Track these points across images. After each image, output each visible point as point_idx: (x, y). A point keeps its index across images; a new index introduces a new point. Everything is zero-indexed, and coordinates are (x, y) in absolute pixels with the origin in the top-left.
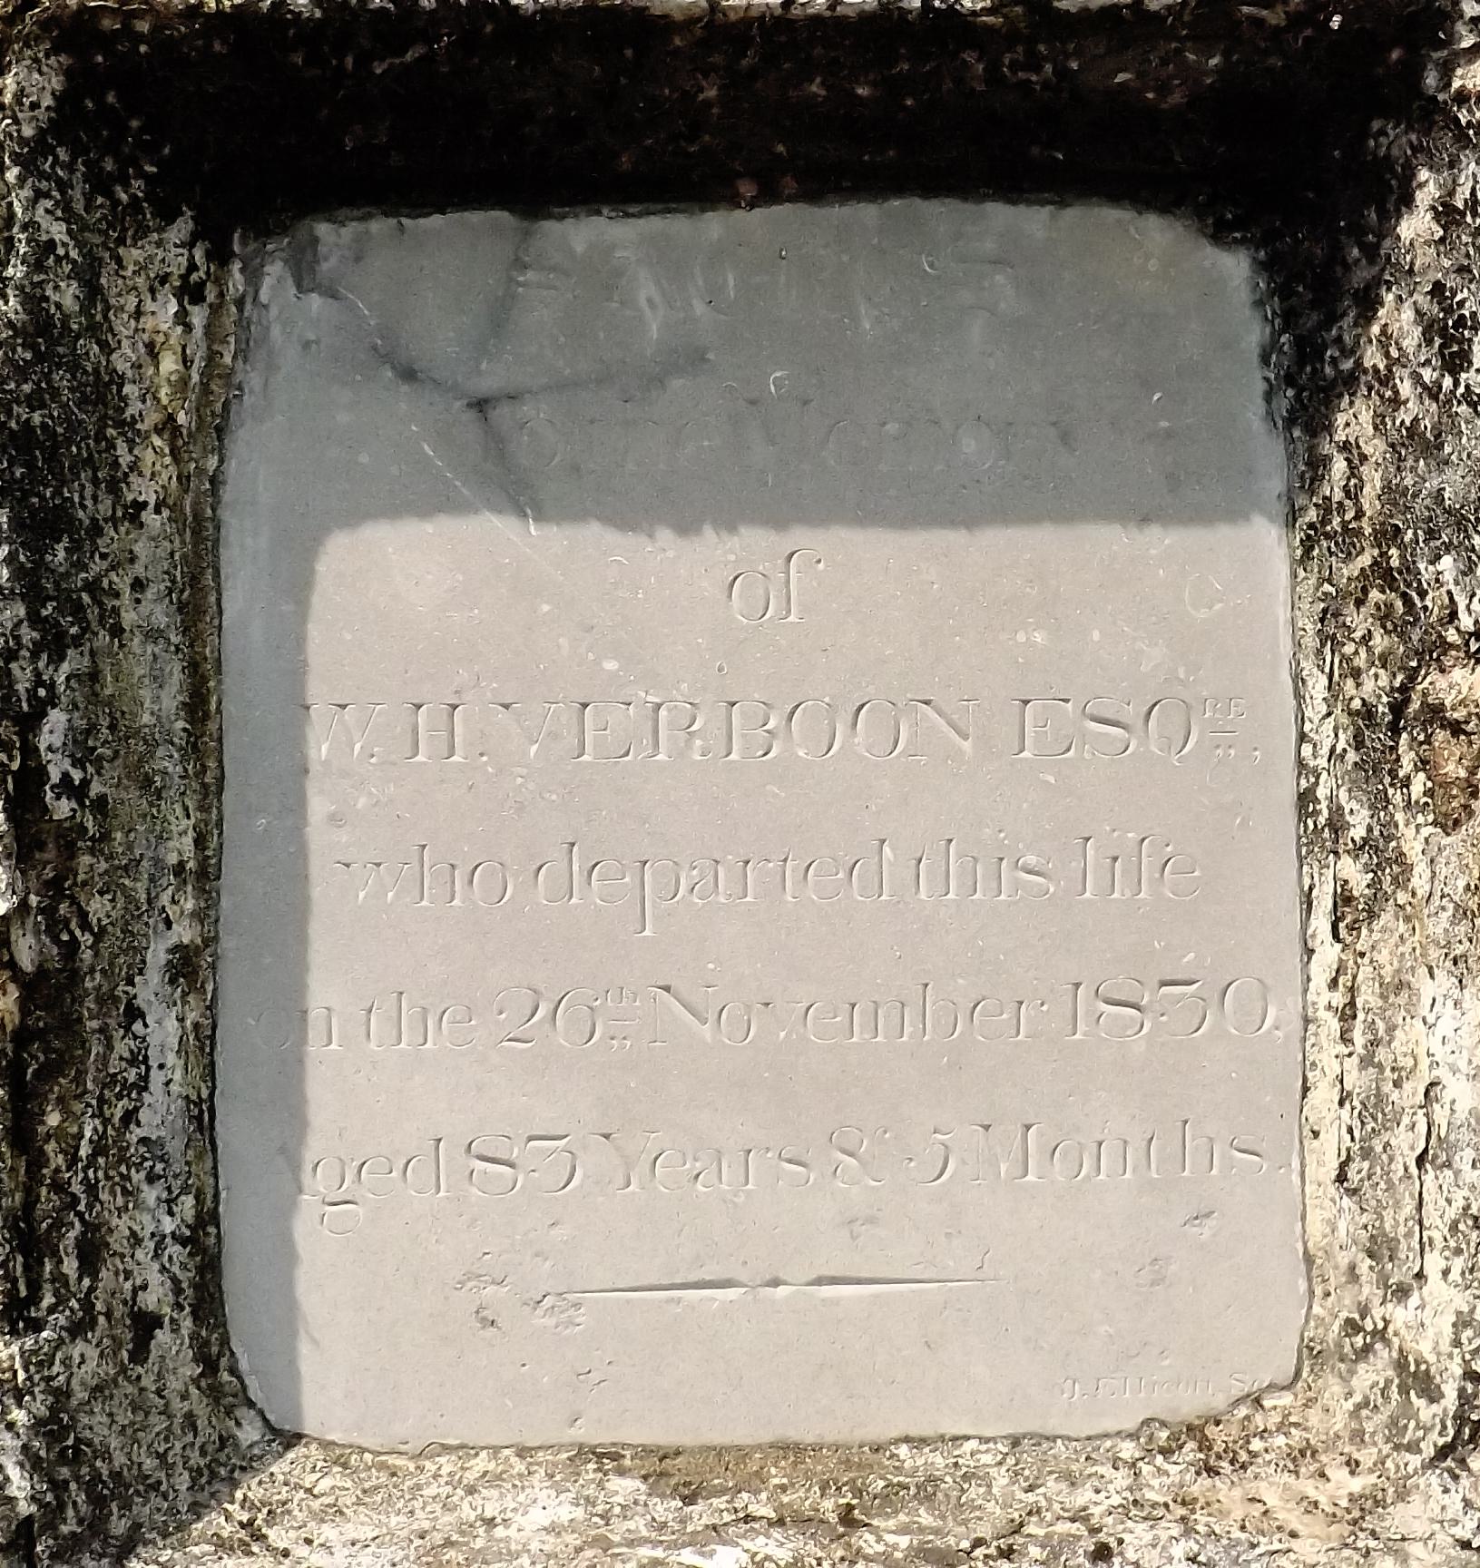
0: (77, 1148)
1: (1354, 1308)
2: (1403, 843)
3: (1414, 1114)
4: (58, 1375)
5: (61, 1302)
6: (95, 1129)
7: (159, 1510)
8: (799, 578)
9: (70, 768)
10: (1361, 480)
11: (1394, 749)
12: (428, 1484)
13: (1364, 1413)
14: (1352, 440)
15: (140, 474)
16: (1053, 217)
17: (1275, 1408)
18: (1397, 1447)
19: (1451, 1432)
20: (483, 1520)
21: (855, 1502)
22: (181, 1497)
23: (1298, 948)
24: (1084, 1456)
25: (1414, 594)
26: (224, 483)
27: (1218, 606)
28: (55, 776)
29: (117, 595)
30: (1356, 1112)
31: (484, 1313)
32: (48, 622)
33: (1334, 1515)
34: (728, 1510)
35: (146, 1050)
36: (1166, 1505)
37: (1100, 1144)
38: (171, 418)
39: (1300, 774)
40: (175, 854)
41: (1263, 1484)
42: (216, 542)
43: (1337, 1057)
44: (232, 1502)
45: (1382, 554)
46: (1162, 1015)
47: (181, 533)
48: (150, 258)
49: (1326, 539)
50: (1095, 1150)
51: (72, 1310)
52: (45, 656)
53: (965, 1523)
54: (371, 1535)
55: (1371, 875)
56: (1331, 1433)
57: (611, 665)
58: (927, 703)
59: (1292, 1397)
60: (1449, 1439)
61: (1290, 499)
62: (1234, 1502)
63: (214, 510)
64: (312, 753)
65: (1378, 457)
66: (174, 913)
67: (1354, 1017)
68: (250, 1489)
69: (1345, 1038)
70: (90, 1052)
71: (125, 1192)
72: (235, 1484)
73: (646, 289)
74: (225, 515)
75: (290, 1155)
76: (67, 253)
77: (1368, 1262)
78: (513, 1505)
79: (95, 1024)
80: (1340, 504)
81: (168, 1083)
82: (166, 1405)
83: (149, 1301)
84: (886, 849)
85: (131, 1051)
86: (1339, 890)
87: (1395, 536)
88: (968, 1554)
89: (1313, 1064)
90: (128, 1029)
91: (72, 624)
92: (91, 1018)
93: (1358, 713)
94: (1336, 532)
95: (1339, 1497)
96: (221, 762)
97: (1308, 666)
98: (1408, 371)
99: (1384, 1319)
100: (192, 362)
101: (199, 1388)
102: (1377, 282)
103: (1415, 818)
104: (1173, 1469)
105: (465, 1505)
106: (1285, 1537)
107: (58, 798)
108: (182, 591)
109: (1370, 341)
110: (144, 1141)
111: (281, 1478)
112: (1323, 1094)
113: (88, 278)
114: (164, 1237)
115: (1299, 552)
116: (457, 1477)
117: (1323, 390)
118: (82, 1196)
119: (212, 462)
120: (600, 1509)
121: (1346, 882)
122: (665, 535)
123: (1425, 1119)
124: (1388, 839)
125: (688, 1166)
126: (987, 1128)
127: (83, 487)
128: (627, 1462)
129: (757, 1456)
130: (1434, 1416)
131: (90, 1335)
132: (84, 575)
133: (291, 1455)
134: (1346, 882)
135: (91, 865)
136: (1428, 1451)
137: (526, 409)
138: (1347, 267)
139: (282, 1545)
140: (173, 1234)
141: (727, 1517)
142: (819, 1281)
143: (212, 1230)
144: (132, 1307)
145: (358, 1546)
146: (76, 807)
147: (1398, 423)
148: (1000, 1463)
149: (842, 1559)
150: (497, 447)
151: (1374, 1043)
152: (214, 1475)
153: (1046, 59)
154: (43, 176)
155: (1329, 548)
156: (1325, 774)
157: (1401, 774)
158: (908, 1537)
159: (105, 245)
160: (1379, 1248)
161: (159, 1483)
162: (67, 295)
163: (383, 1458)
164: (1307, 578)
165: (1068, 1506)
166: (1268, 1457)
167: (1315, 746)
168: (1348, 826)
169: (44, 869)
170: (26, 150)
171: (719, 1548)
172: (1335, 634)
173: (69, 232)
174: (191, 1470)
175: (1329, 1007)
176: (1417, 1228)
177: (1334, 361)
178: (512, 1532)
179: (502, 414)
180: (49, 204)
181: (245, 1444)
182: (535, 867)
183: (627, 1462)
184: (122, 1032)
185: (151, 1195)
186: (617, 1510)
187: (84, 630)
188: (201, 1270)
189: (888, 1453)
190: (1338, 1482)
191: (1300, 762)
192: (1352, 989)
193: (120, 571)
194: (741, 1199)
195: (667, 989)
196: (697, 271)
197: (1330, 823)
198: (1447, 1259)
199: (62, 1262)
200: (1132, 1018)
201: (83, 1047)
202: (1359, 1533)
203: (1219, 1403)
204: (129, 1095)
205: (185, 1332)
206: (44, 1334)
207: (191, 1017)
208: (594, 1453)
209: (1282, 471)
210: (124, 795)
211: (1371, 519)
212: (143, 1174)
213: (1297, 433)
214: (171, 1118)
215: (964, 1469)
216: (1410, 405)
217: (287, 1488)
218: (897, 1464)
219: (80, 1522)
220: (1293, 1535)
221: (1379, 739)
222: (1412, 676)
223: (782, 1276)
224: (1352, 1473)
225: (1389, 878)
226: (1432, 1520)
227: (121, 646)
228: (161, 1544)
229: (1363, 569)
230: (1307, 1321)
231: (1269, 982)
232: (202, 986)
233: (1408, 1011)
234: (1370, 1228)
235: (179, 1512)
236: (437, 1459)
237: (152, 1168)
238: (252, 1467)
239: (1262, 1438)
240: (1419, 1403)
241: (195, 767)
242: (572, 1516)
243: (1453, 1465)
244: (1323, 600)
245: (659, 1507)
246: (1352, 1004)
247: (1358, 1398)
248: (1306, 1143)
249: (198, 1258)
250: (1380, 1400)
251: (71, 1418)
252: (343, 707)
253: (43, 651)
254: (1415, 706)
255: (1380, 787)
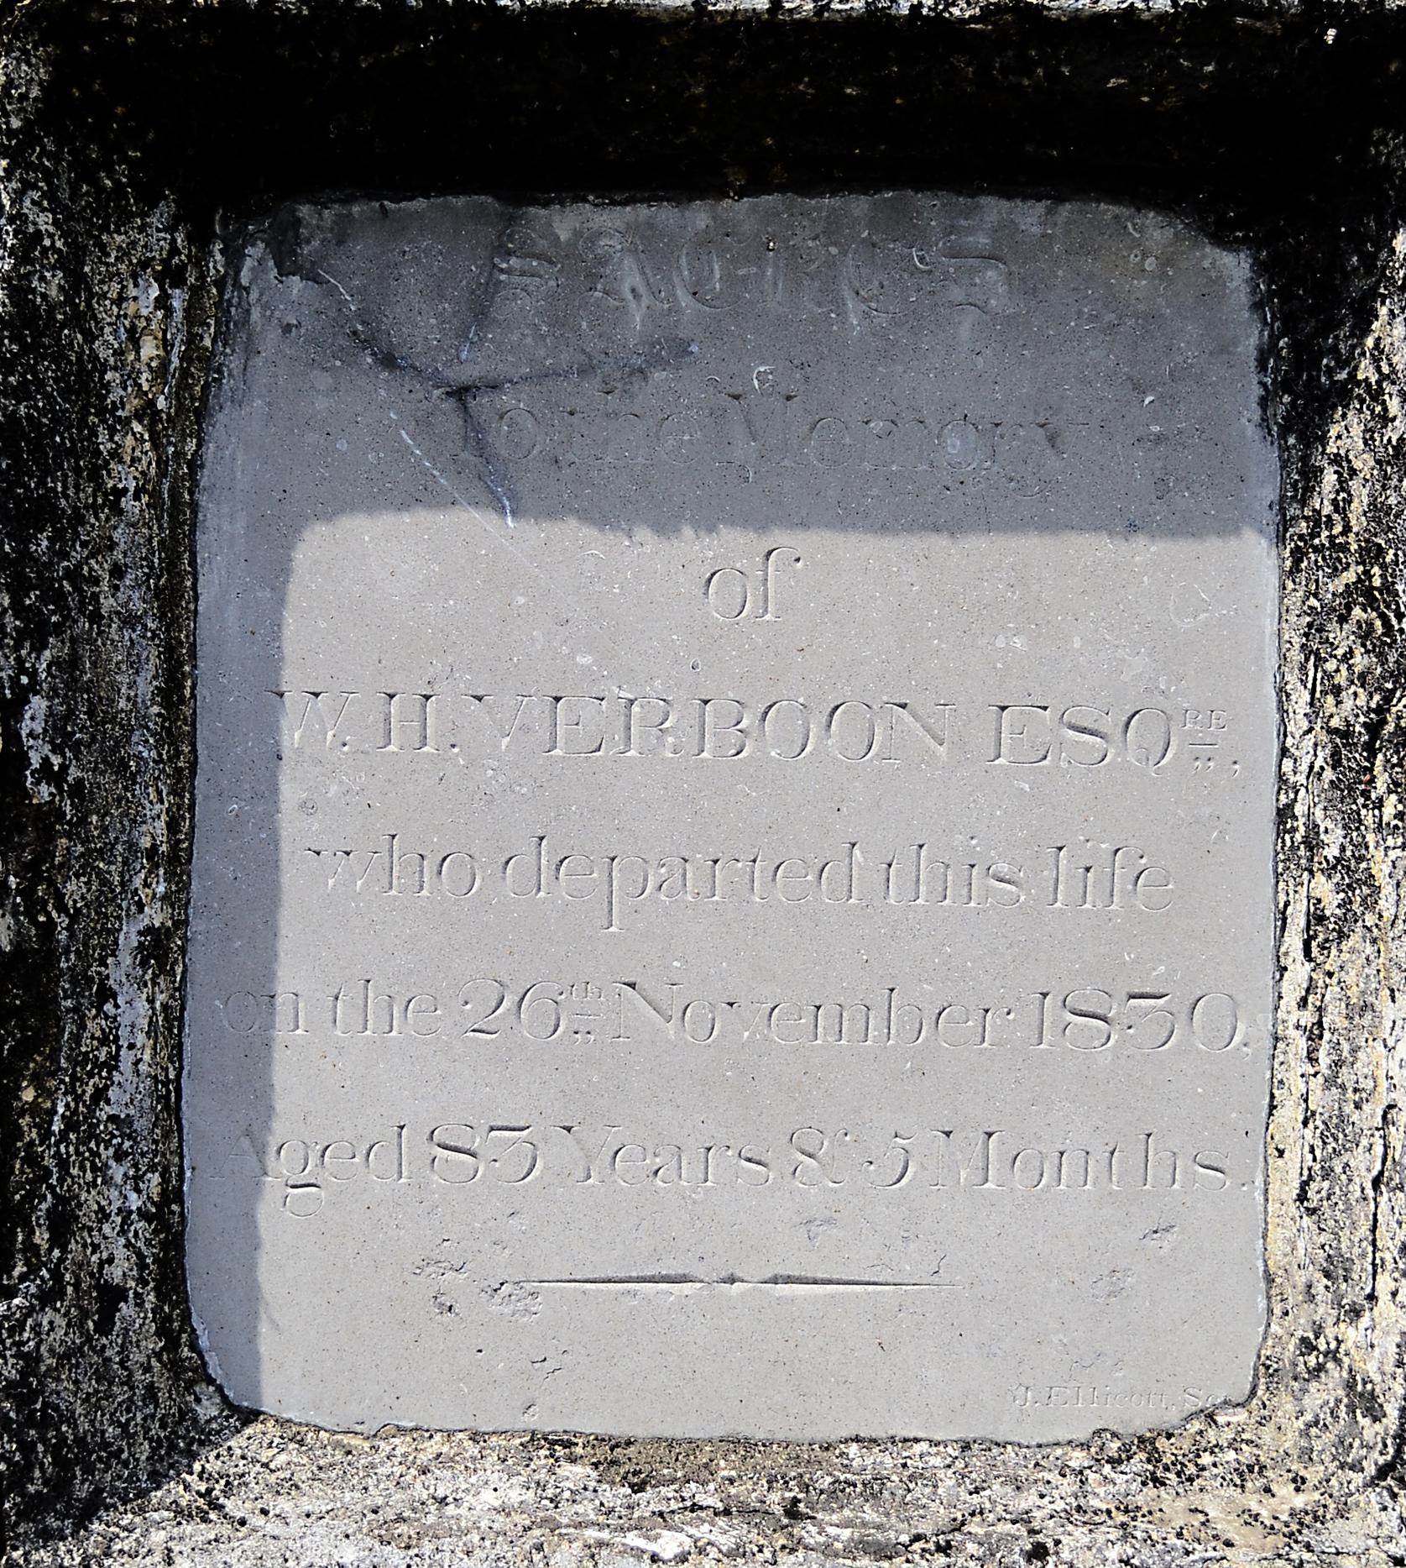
0: (51, 1123)
1: (1308, 1327)
2: (1372, 865)
3: (1372, 1135)
4: (29, 1340)
5: (32, 1271)
6: (67, 1106)
7: (120, 1477)
8: (776, 576)
9: (50, 755)
10: (1350, 495)
11: (1371, 770)
12: (382, 1463)
13: (1314, 1431)
14: (1342, 452)
15: (121, 461)
16: (1050, 211)
17: (1229, 1424)
18: (1342, 1466)
19: (1391, 1450)
20: (434, 1498)
21: (801, 1496)
22: (142, 1465)
23: (1271, 966)
24: (1033, 1462)
25: (1392, 615)
26: (202, 466)
27: (1203, 616)
28: (35, 761)
29: (96, 581)
30: (1318, 1131)
31: (442, 1299)
32: (32, 611)
33: (1272, 1528)
34: (675, 1498)
35: (117, 1029)
36: (1109, 1512)
37: (1062, 1154)
38: (152, 403)
39: (1280, 788)
40: (149, 838)
41: (1207, 1497)
42: (193, 527)
43: (1302, 1076)
44: (191, 1473)
45: (1366, 572)
46: (1130, 1027)
47: (159, 519)
48: (133, 244)
49: (1314, 552)
50: (1056, 1161)
51: (42, 1278)
52: (27, 645)
53: (908, 1520)
54: (324, 1509)
55: (1342, 895)
56: (1281, 1451)
57: (584, 660)
58: (903, 706)
59: (1246, 1414)
60: (1389, 1458)
61: (1282, 511)
62: (1177, 1512)
63: (191, 493)
64: (285, 742)
65: (1366, 473)
66: (147, 896)
67: (1321, 1037)
68: (208, 1461)
69: (1312, 1059)
70: (64, 1030)
71: (94, 1169)
72: (194, 1456)
73: (630, 276)
74: (203, 499)
75: (255, 1136)
76: (53, 243)
77: (1325, 1281)
78: (464, 1487)
79: (69, 1003)
80: (1329, 517)
81: (138, 1062)
82: (130, 1376)
83: (115, 1274)
84: (857, 851)
85: (103, 1030)
86: (1312, 909)
87: (1377, 557)
88: (906, 1547)
89: (1281, 1082)
90: (100, 1009)
91: (54, 612)
92: (65, 998)
93: (1336, 731)
94: (1323, 545)
95: (1282, 1512)
96: (193, 745)
97: (1292, 678)
98: (1397, 388)
99: (1337, 1339)
100: (173, 346)
101: (160, 1361)
102: (1372, 295)
103: (1385, 840)
104: (1119, 1479)
105: (418, 1485)
106: (1220, 1545)
107: (37, 783)
108: (159, 578)
109: (1363, 354)
110: (113, 1118)
111: (239, 1452)
112: (1290, 1113)
113: (71, 264)
114: (131, 1212)
115: (1288, 563)
116: (411, 1458)
117: (1318, 399)
118: (55, 1170)
119: (191, 445)
120: (550, 1493)
121: (1319, 901)
122: (643, 534)
123: (1382, 1141)
124: (1361, 859)
125: (648, 1161)
126: (948, 1134)
127: (65, 476)
128: (579, 1450)
129: (708, 1448)
130: (1377, 1433)
131: (58, 1304)
132: (66, 563)
133: (249, 1431)
134: (1319, 901)
135: (68, 849)
136: (1371, 1470)
137: (506, 399)
138: (1347, 276)
139: (239, 1515)
140: (139, 1209)
141: (674, 1505)
142: (775, 1280)
143: (174, 1207)
144: (99, 1280)
145: (313, 1517)
146: (54, 791)
147: (1385, 439)
148: (949, 1466)
149: (783, 1547)
150: (476, 438)
151: (1338, 1064)
152: (172, 1447)
153: (1038, 64)
154: (30, 167)
155: (1316, 561)
156: (1303, 790)
157: (1373, 796)
158: (850, 1530)
159: (90, 235)
160: (1334, 1269)
161: (121, 1451)
162: (51, 285)
163: (339, 1437)
164: (1295, 590)
165: (1010, 1509)
166: (1215, 1471)
167: (1296, 760)
168: (1322, 845)
169: (24, 852)
170: (13, 142)
171: (665, 1533)
172: (1318, 649)
173: (55, 223)
174: (151, 1440)
175: (1298, 1027)
176: (1370, 1249)
177: (1330, 372)
178: (463, 1511)
179: (481, 404)
180: (36, 195)
181: (203, 1419)
182: (504, 860)
183: (579, 1450)
184: (94, 1011)
185: (118, 1172)
186: (567, 1494)
187: (65, 618)
188: (164, 1245)
189: (837, 1452)
190: (1283, 1497)
191: (1280, 777)
192: (1319, 1009)
193: (100, 558)
194: (699, 1197)
195: (632, 985)
196: (683, 261)
197: (1306, 841)
198: (1396, 1280)
199: (34, 1233)
200: (1099, 1030)
201: (58, 1026)
202: (1293, 1545)
203: (1172, 1418)
204: (99, 1073)
205: (148, 1306)
206: (16, 1301)
207: (161, 998)
208: (546, 1440)
209: (1276, 478)
210: (100, 779)
211: (1357, 534)
212: (111, 1151)
213: (1292, 441)
214: (139, 1097)
215: (912, 1470)
216: (1397, 423)
217: (245, 1462)
218: (845, 1462)
219: (45, 1484)
220: (1229, 1544)
221: (1355, 758)
222: (1388, 697)
223: (739, 1274)
224: (1297, 1490)
225: (1358, 899)
226: (1368, 1536)
227: (100, 633)
228: (122, 1509)
229: (1347, 585)
230: (1265, 1339)
231: (1240, 997)
232: (172, 969)
233: (1371, 1033)
234: (1327, 1248)
235: (139, 1480)
236: (392, 1440)
237: (120, 1145)
238: (210, 1441)
239: (1212, 1452)
240: (1364, 1422)
241: (168, 752)
242: (523, 1498)
243: (1392, 1483)
244: (1309, 615)
245: (607, 1494)
246: (1320, 1024)
247: (1309, 1417)
248: (1270, 1161)
249: (162, 1236)
250: (1329, 1420)
251: (40, 1383)
252: (316, 695)
253: (26, 640)
254: (1390, 727)
255: (1354, 807)
